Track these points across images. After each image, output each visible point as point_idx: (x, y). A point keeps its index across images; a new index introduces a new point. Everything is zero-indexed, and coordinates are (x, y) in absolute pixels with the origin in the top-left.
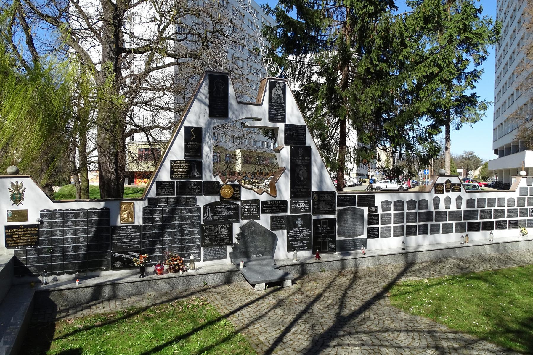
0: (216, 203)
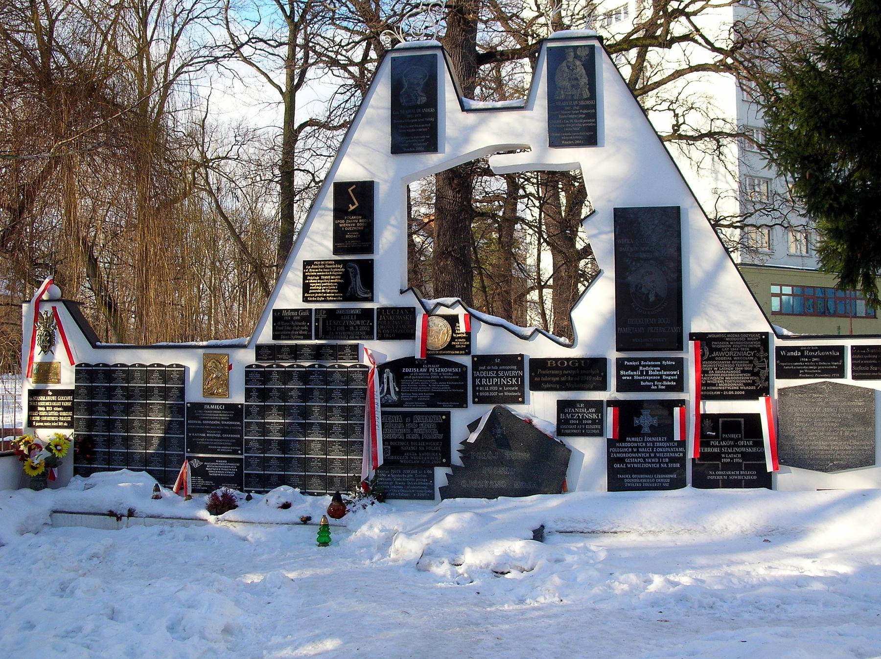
0: (409, 361)
